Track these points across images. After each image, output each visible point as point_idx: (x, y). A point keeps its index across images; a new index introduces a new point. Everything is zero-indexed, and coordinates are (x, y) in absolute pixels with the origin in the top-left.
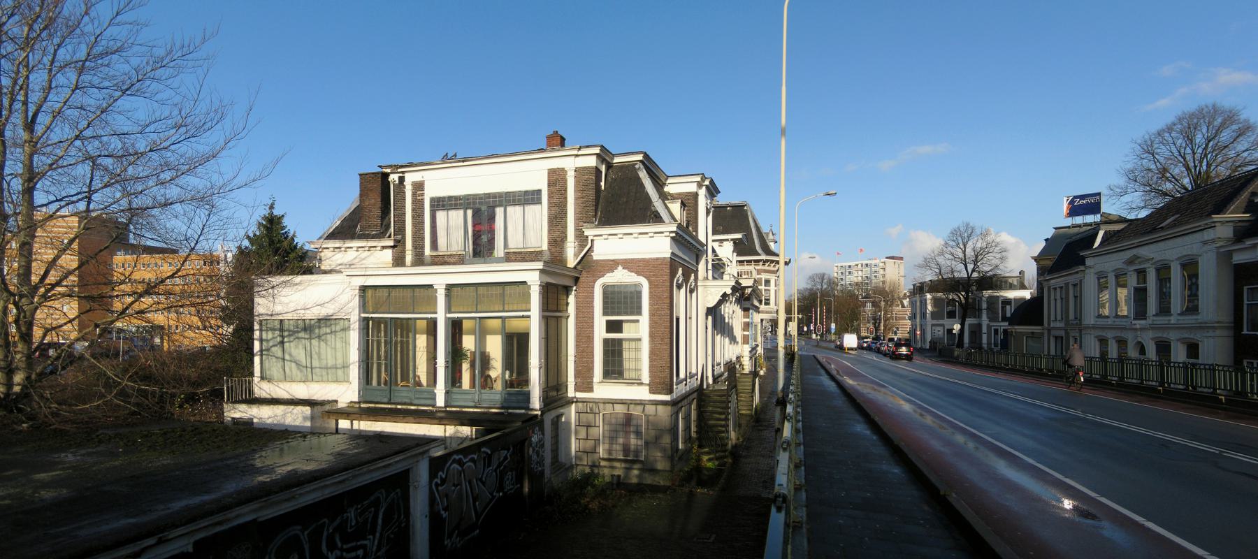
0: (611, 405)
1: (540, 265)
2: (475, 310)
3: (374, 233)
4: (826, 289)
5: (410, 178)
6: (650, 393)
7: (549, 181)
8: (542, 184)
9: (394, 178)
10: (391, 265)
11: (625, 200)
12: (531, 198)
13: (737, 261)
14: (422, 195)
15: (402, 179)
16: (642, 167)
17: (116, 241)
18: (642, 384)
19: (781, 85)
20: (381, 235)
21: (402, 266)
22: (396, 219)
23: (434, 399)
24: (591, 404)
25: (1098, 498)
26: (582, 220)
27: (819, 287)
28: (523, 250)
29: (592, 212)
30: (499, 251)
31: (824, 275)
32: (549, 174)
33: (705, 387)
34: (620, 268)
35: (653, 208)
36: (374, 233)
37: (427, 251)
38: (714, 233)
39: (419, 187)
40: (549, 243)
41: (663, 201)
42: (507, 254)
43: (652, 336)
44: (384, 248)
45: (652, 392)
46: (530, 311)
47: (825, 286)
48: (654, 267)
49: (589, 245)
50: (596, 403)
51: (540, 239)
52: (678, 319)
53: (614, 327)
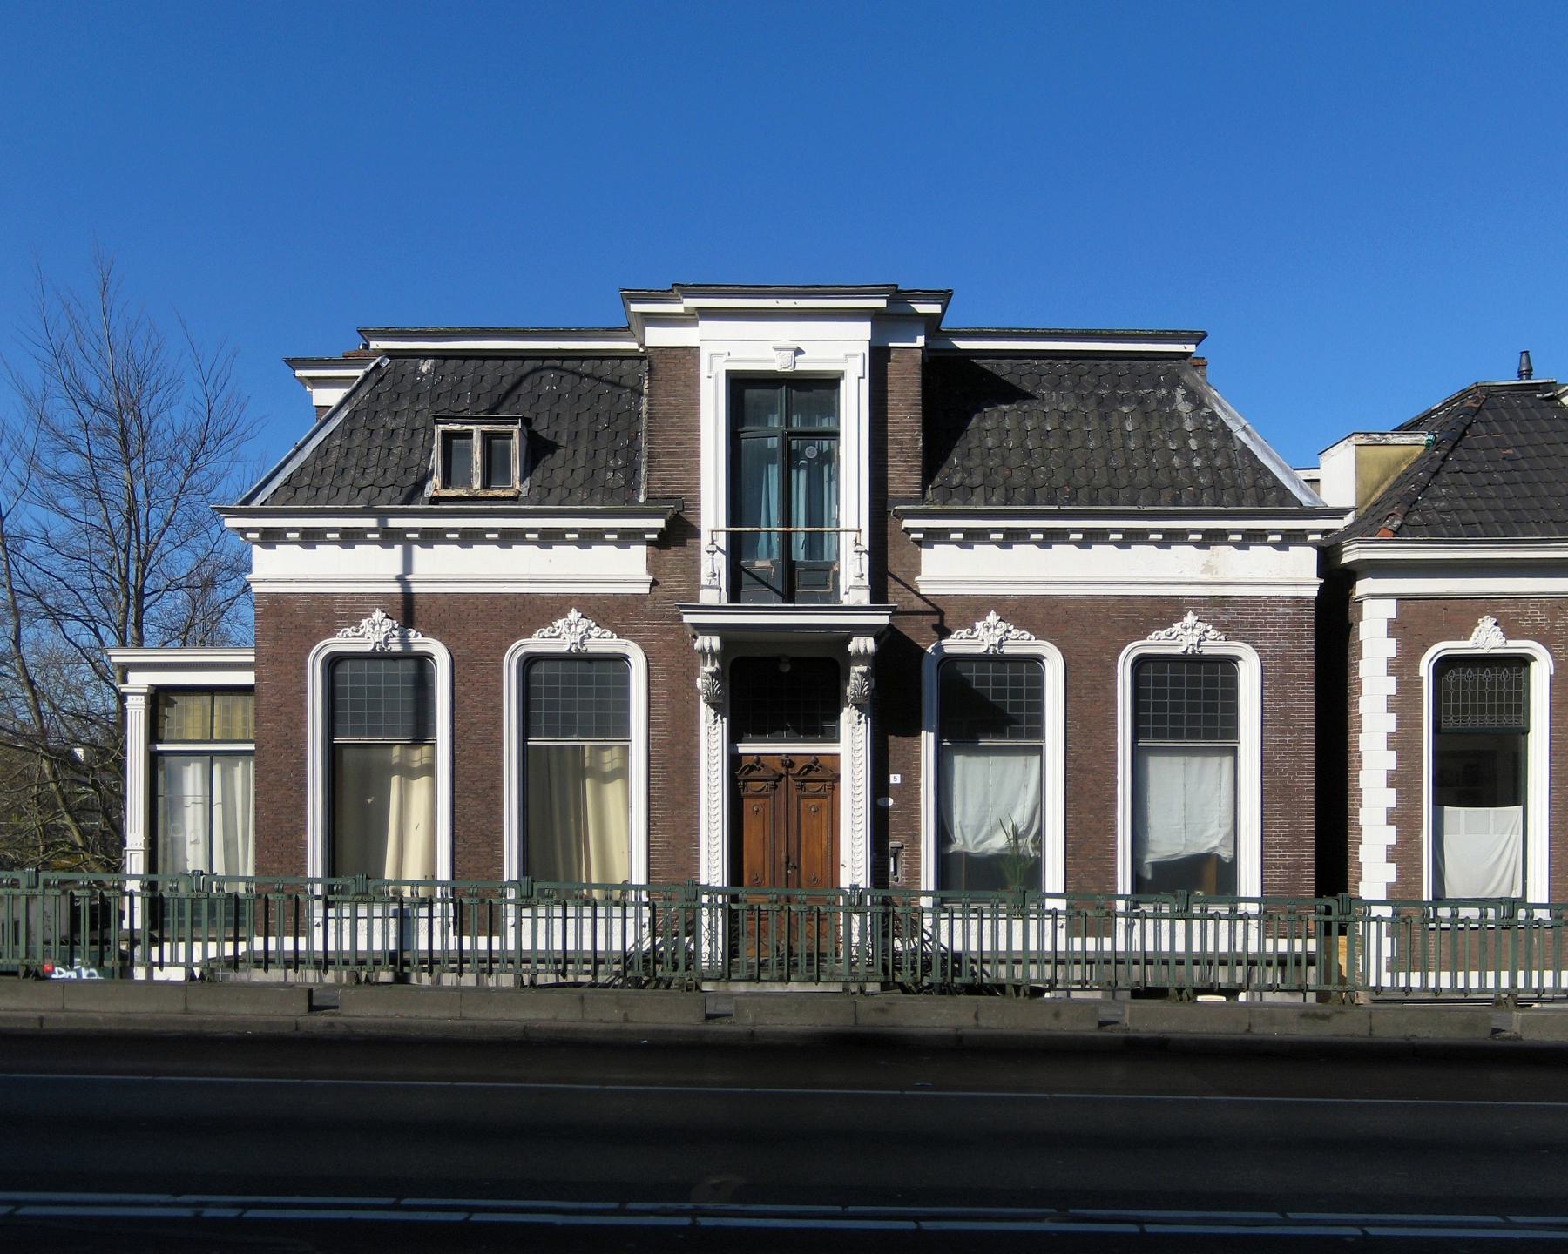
19: (566, 1084)
26: (1440, 801)
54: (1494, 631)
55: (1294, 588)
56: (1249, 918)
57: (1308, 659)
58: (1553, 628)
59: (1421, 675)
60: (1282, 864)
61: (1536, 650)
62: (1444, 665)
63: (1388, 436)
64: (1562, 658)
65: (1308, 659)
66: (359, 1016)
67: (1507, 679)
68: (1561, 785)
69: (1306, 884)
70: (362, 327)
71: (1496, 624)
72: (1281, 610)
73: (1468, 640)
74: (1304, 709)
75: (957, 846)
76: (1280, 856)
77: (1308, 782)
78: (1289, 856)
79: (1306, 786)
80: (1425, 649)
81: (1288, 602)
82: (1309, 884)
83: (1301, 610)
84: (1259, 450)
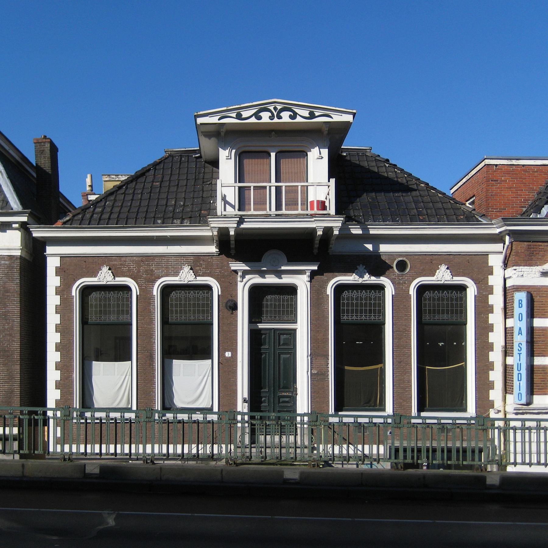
19: (34, 508)
37: (187, 157)
54: (447, 272)
55: (9, 251)
56: (531, 430)
57: (16, 287)
58: (139, 272)
59: (327, 294)
60: (4, 390)
61: (468, 282)
62: (422, 289)
63: (119, 176)
64: (144, 286)
65: (16, 287)
67: (374, 296)
68: (143, 350)
69: (16, 400)
71: (448, 268)
72: (3, 262)
73: (96, 277)
74: (15, 312)
76: (2, 386)
77: (16, 348)
78: (7, 386)
79: (16, 351)
80: (75, 281)
81: (7, 258)
82: (17, 400)
83: (13, 262)
84: (4, 183)
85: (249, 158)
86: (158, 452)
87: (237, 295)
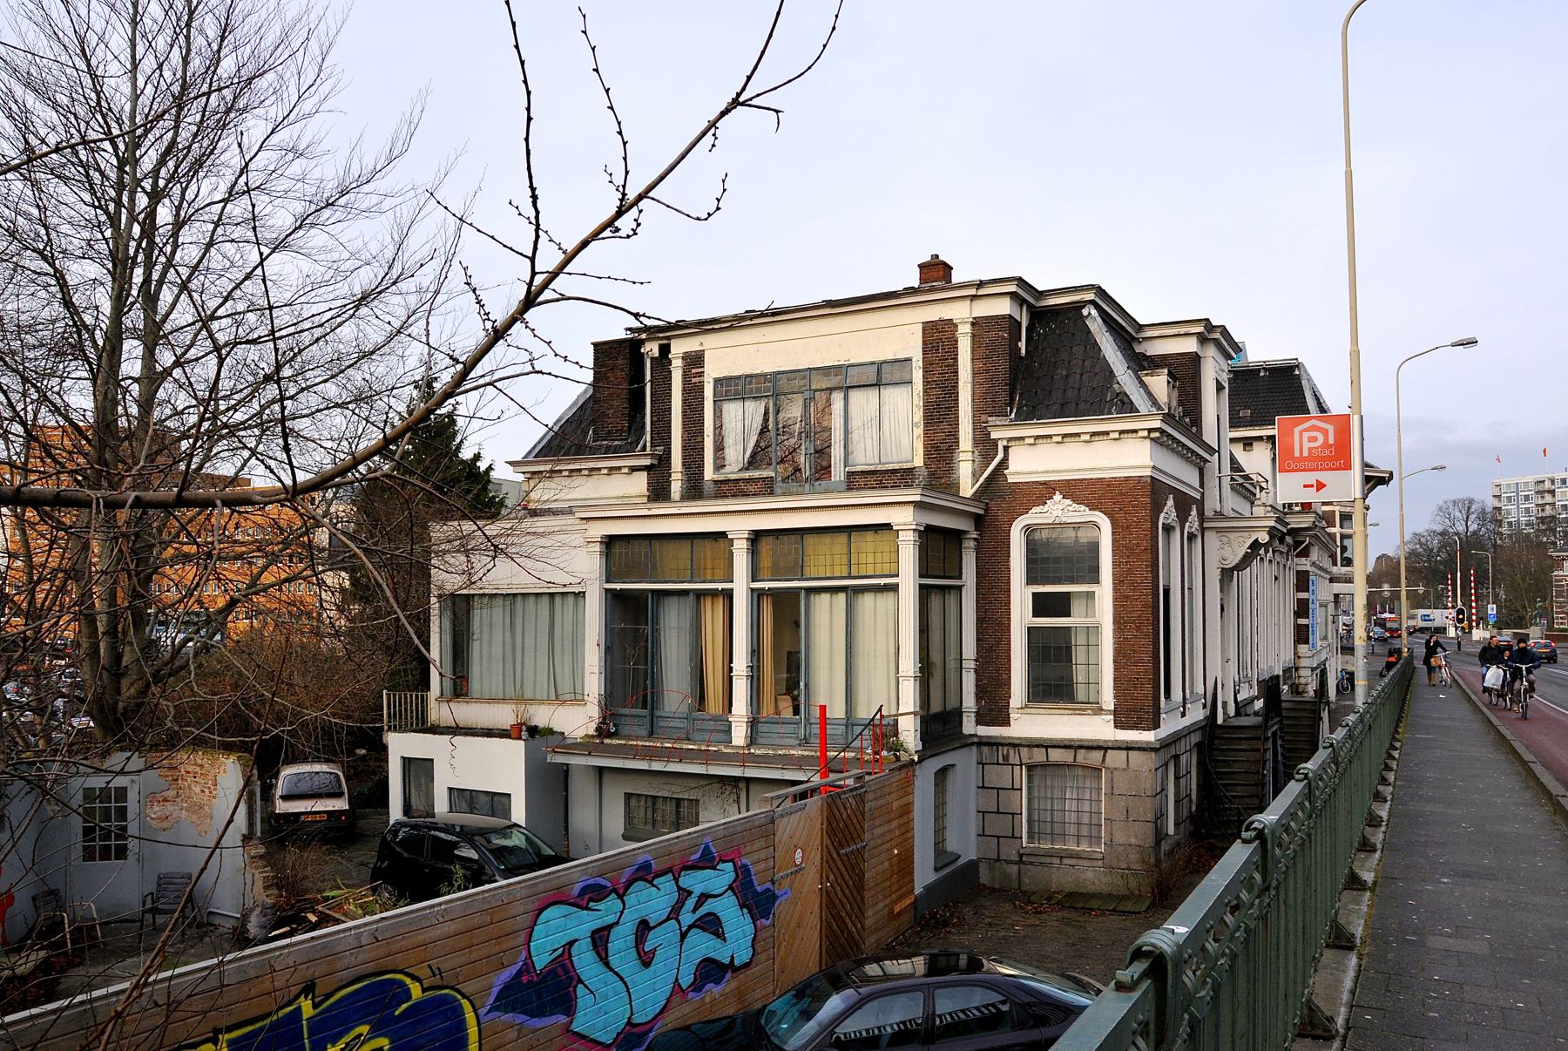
0: (1044, 750)
1: (914, 495)
2: (845, 574)
3: (616, 443)
4: (1474, 533)
5: (679, 348)
6: (1116, 727)
7: (924, 343)
8: (912, 347)
9: (652, 349)
10: (645, 500)
11: (1064, 373)
12: (881, 376)
13: (898, 576)
14: (701, 374)
15: (665, 350)
16: (1094, 312)
17: (435, 265)
18: (1099, 711)
20: (629, 448)
21: (605, 343)
22: (655, 419)
23: (729, 731)
24: (1005, 749)
25: (62, 1002)
26: (986, 407)
27: (1461, 528)
28: (879, 468)
29: (1003, 397)
30: (838, 473)
31: (1471, 502)
32: (924, 330)
33: (1220, 721)
34: (1058, 497)
35: (1116, 386)
36: (616, 443)
37: (709, 473)
38: (1235, 422)
39: (695, 361)
40: (927, 453)
41: (1135, 373)
42: (850, 475)
43: (1118, 620)
44: (634, 469)
45: (1119, 725)
46: (898, 576)
47: (1473, 527)
48: (1121, 494)
49: (1000, 455)
50: (1014, 746)
51: (908, 448)
52: (1167, 592)
53: (1043, 605)
66: (889, 463)
70: (1443, 471)
75: (916, 284)
85: (856, 711)
86: (645, 474)
87: (1008, 603)
